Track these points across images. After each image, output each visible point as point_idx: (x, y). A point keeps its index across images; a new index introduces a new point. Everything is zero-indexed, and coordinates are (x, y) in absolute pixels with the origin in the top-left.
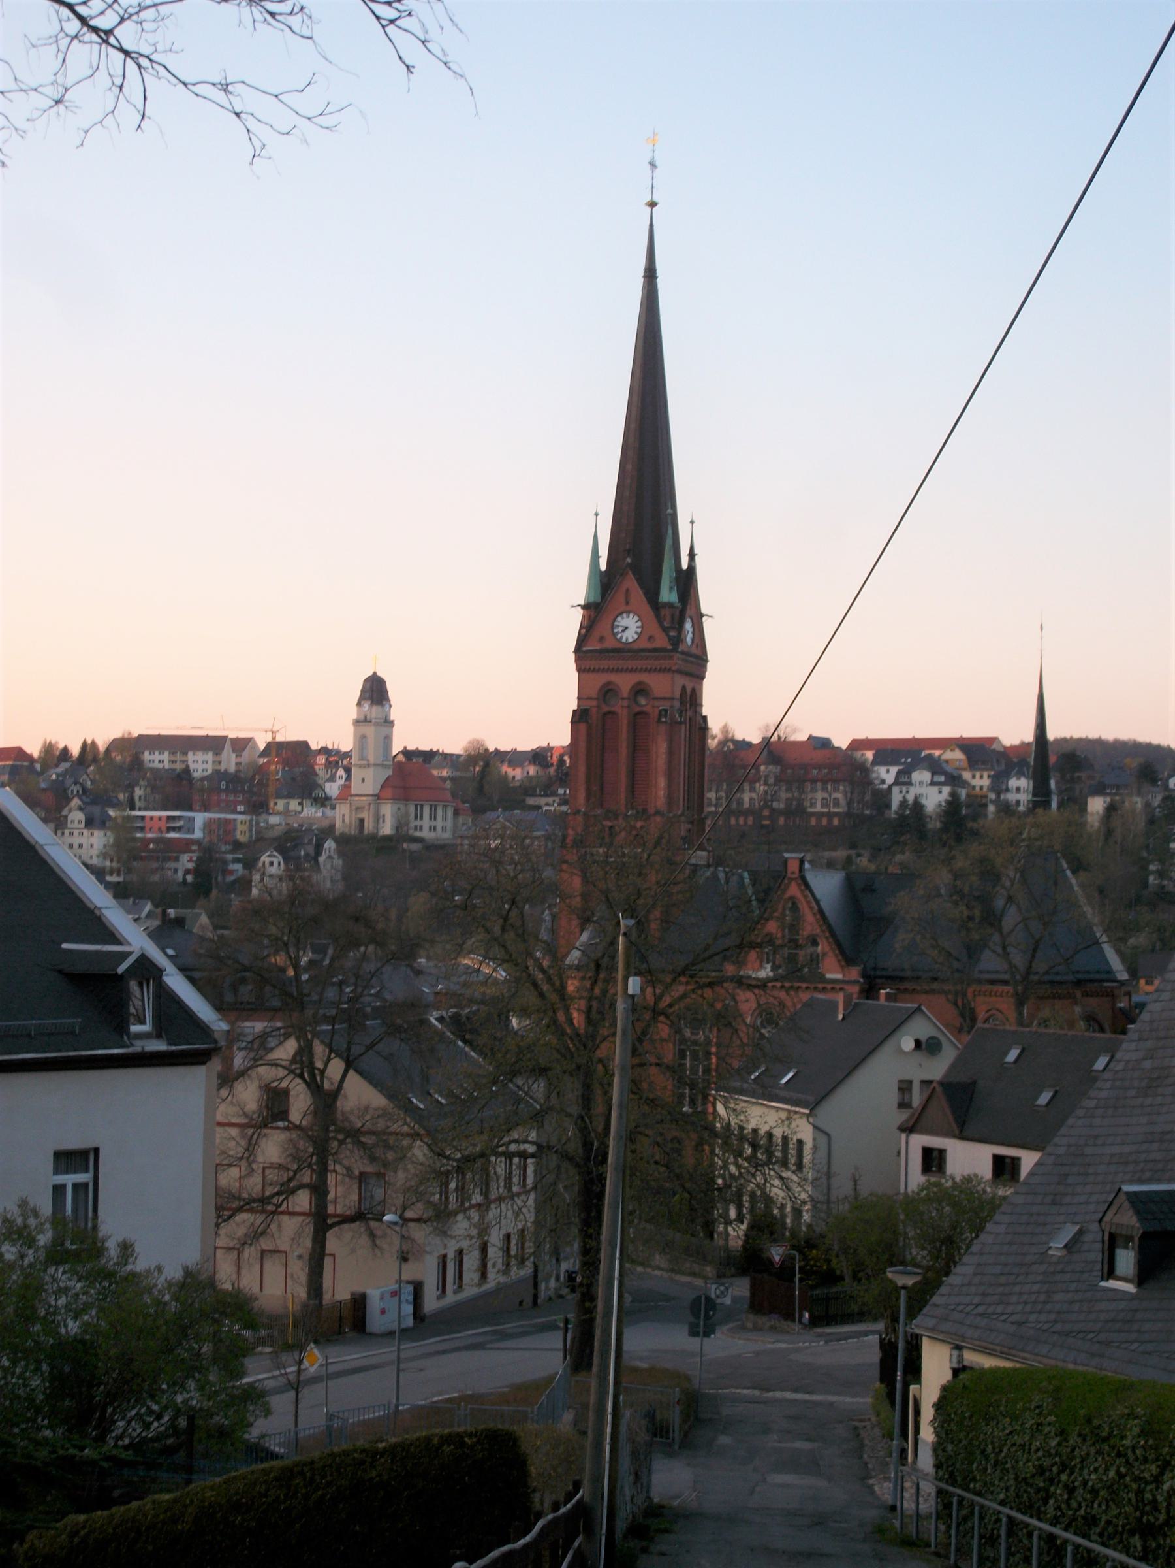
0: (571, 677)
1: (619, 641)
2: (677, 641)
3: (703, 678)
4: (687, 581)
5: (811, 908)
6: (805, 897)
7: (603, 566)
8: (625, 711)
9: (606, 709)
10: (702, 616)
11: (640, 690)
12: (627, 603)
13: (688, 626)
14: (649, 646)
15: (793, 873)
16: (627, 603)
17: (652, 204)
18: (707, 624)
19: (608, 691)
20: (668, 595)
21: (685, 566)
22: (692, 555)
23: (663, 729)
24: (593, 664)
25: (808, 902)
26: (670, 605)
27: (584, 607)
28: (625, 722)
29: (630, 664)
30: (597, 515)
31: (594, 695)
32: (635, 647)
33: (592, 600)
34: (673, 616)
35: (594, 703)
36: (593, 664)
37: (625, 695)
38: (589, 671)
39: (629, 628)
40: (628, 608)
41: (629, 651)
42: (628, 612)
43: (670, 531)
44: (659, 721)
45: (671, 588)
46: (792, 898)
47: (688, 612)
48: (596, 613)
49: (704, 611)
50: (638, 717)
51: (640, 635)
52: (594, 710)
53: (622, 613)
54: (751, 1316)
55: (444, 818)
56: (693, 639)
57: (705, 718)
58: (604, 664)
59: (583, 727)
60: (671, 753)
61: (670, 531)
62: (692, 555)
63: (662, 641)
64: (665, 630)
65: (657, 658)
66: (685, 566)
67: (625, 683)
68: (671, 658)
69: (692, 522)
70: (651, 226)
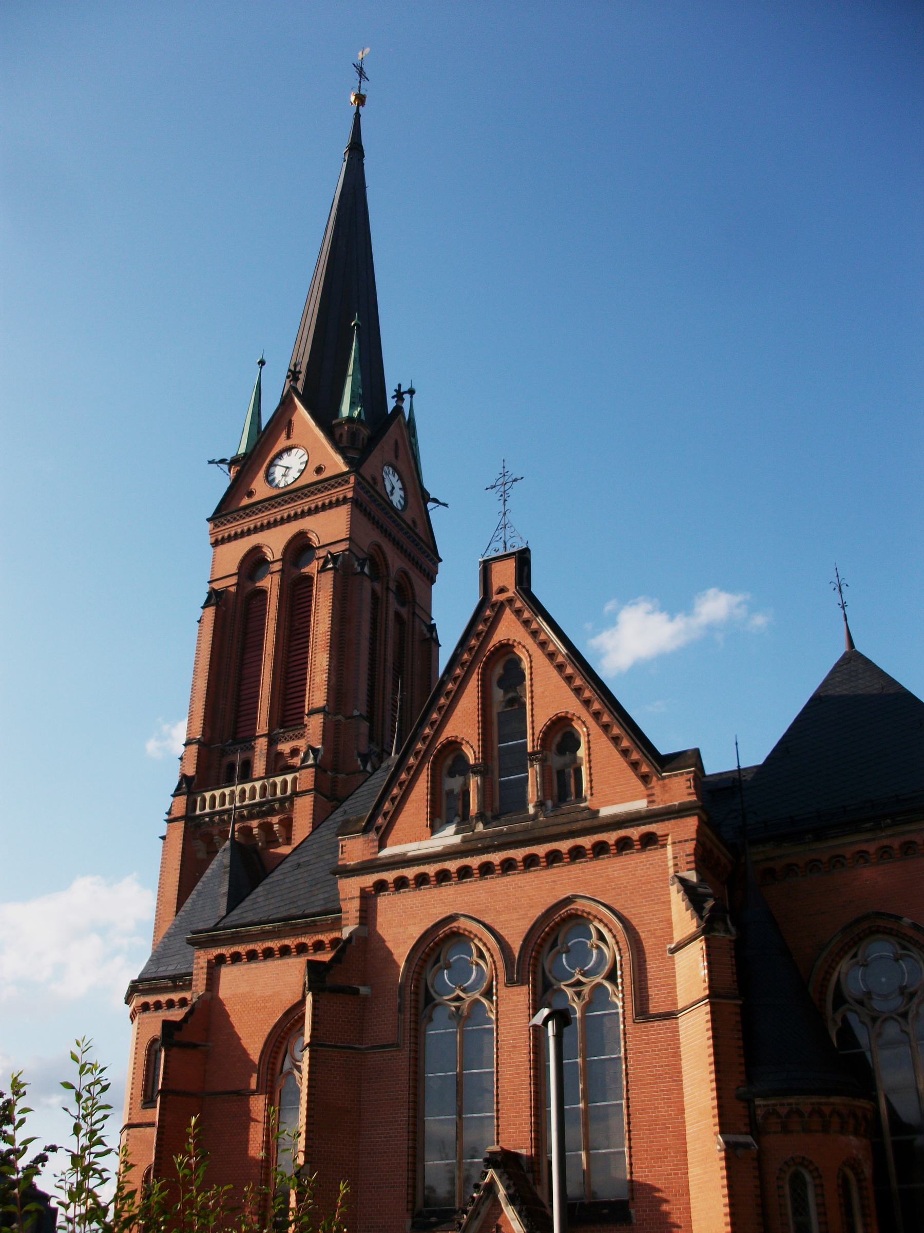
3: (433, 581)
5: (551, 656)
6: (535, 634)
9: (249, 587)
10: (425, 497)
12: (288, 437)
15: (502, 590)
19: (254, 562)
25: (543, 645)
30: (262, 363)
46: (506, 648)
67: (274, 543)
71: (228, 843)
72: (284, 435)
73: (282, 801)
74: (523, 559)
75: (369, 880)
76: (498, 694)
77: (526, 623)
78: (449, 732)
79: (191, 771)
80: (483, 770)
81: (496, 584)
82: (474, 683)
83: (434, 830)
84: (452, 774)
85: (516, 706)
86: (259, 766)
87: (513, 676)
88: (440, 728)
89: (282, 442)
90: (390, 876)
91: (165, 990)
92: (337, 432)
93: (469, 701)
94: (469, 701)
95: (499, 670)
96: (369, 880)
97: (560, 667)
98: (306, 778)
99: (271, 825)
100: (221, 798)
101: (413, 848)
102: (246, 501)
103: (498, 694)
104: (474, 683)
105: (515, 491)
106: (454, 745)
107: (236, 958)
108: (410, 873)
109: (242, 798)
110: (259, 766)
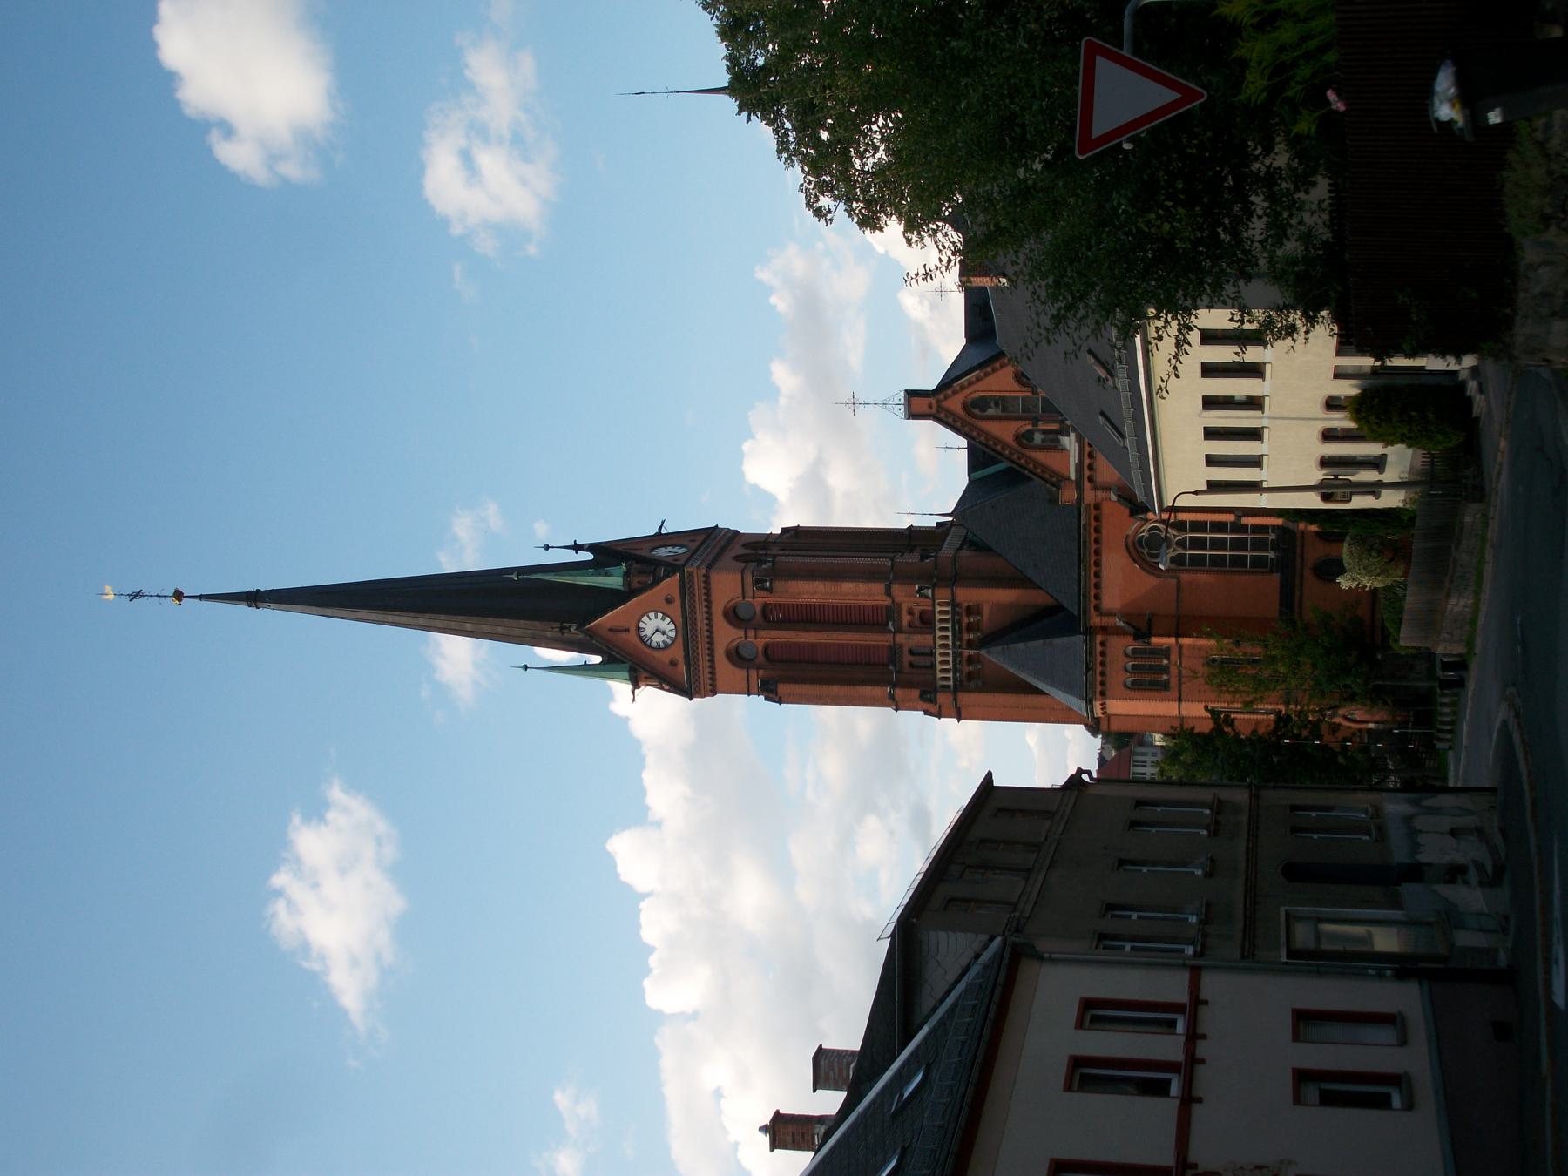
0: (754, 697)
1: (674, 640)
2: (672, 567)
3: (737, 532)
4: (606, 554)
5: (978, 379)
6: (962, 388)
7: (596, 659)
8: (761, 633)
9: (761, 659)
10: (659, 534)
11: (734, 616)
12: (627, 630)
13: (662, 552)
14: (678, 603)
15: (930, 406)
16: (627, 630)
17: (178, 595)
18: (670, 528)
19: (737, 657)
20: (613, 580)
21: (589, 556)
22: (577, 547)
23: (779, 585)
24: (704, 676)
25: (970, 384)
26: (626, 575)
27: (636, 686)
28: (774, 633)
29: (702, 626)
30: (526, 667)
31: (744, 673)
32: (680, 621)
33: (626, 675)
34: (641, 572)
35: (753, 673)
36: (704, 676)
37: (742, 633)
38: (713, 679)
39: (657, 627)
40: (633, 629)
41: (685, 624)
42: (638, 629)
43: (539, 576)
44: (770, 590)
45: (607, 574)
46: (965, 406)
47: (644, 553)
48: (641, 668)
49: (653, 531)
50: (770, 618)
51: (665, 615)
52: (761, 672)
53: (641, 638)
54: (1523, 330)
55: (1145, 754)
56: (682, 546)
57: (784, 530)
58: (704, 661)
59: (783, 689)
60: (811, 574)
61: (539, 576)
62: (577, 547)
63: (671, 585)
64: (656, 582)
65: (692, 595)
66: (589, 556)
67: (726, 635)
68: (690, 574)
69: (547, 547)
70: (201, 597)
71: (983, 652)
72: (624, 635)
73: (954, 613)
74: (911, 394)
75: (1087, 485)
76: (991, 412)
77: (955, 393)
78: (1010, 439)
79: (916, 693)
80: (1035, 421)
81: (925, 410)
82: (984, 425)
83: (1064, 450)
84: (1032, 439)
85: (1001, 402)
86: (918, 640)
87: (982, 403)
88: (1005, 445)
89: (632, 636)
90: (1087, 473)
91: (1094, 677)
92: (635, 585)
93: (994, 428)
94: (994, 428)
95: (976, 411)
96: (1087, 485)
97: (987, 375)
98: (943, 594)
99: (969, 624)
100: (944, 664)
101: (1073, 460)
102: (682, 668)
103: (991, 412)
104: (984, 425)
105: (861, 398)
106: (1018, 438)
107: (1097, 597)
108: (1087, 461)
109: (946, 646)
110: (918, 640)
